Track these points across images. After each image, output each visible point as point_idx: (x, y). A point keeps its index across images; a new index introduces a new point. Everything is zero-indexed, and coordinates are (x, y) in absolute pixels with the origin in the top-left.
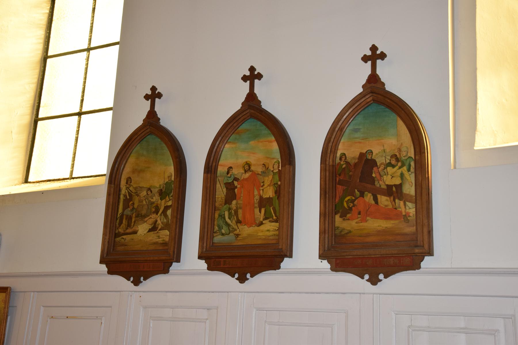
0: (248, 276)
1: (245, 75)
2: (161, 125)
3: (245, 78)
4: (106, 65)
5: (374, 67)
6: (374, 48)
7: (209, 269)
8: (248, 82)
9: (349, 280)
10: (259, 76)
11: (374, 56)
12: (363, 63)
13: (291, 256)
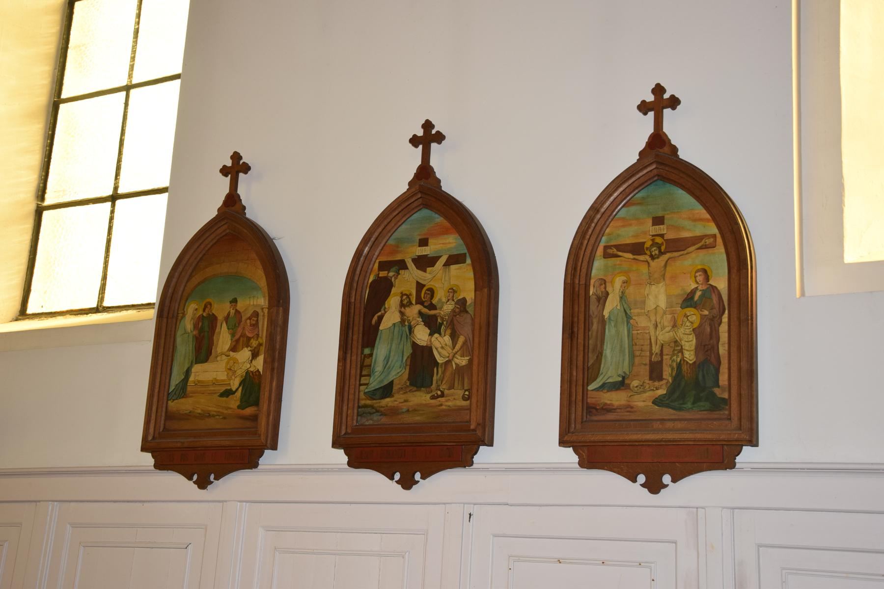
0: (418, 476)
1: (415, 136)
2: (247, 219)
3: (415, 141)
4: (158, 114)
5: (658, 122)
6: (658, 90)
7: (350, 464)
8: (421, 147)
9: (608, 483)
10: (440, 138)
11: (660, 102)
12: (641, 114)
13: (491, 444)
